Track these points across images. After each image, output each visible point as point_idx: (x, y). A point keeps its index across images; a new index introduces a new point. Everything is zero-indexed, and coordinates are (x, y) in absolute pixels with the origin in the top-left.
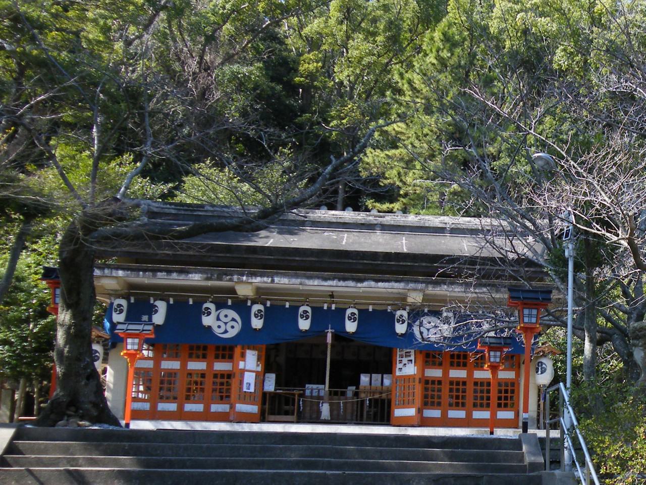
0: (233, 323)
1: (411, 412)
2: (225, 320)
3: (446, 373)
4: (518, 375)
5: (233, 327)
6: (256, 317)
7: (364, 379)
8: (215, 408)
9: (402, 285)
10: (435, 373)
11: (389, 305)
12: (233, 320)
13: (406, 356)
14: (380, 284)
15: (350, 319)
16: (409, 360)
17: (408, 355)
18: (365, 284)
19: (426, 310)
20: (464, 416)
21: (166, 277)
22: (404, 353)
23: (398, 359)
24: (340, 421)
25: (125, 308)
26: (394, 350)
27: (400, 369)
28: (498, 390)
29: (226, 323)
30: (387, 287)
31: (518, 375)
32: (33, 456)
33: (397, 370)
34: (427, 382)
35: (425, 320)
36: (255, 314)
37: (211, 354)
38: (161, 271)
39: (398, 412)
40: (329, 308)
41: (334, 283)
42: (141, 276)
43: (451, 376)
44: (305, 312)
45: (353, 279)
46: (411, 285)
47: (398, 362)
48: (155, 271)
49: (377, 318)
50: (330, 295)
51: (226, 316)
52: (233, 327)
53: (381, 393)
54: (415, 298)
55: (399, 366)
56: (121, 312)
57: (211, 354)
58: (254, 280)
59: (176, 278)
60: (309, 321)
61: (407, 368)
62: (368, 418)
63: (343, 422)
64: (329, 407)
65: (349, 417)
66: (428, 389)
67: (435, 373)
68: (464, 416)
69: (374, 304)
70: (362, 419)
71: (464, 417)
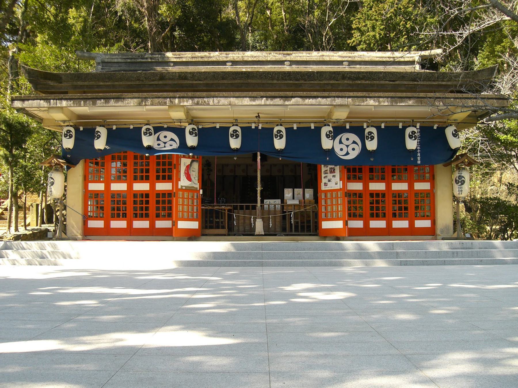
0: (354, 146)
1: (338, 224)
2: (347, 143)
3: (366, 186)
4: (433, 186)
5: (353, 149)
6: (410, 138)
7: (288, 193)
8: (160, 224)
9: (328, 101)
10: (357, 186)
11: (401, 122)
12: (354, 142)
13: (331, 172)
14: (308, 101)
15: (410, 137)
16: (333, 176)
17: (332, 171)
18: (294, 100)
19: (348, 127)
20: (407, 226)
21: (104, 105)
22: (328, 169)
23: (323, 175)
24: (271, 233)
25: (284, 133)
26: (318, 166)
27: (326, 184)
28: (157, 207)
29: (347, 146)
30: (314, 103)
31: (433, 186)
32: (240, 260)
33: (323, 184)
34: (350, 195)
35: (345, 136)
36: (409, 136)
37: (366, 174)
38: (100, 99)
39: (326, 225)
40: (257, 128)
41: (263, 101)
42: (82, 105)
43: (370, 189)
44: (279, 131)
45: (281, 97)
46: (338, 101)
47: (323, 178)
48: (94, 99)
49: (304, 136)
50: (256, 116)
51: (348, 139)
52: (353, 149)
53: (305, 206)
54: (341, 115)
55: (324, 181)
56: (372, 138)
57: (366, 174)
58: (185, 104)
59: (114, 105)
60: (284, 139)
61: (332, 181)
62: (296, 230)
63: (249, 233)
64: (262, 222)
65: (278, 229)
66: (165, 209)
67: (357, 186)
68: (407, 226)
69: (386, 122)
70: (309, 230)
71: (362, 227)
